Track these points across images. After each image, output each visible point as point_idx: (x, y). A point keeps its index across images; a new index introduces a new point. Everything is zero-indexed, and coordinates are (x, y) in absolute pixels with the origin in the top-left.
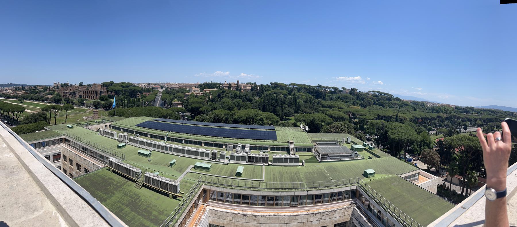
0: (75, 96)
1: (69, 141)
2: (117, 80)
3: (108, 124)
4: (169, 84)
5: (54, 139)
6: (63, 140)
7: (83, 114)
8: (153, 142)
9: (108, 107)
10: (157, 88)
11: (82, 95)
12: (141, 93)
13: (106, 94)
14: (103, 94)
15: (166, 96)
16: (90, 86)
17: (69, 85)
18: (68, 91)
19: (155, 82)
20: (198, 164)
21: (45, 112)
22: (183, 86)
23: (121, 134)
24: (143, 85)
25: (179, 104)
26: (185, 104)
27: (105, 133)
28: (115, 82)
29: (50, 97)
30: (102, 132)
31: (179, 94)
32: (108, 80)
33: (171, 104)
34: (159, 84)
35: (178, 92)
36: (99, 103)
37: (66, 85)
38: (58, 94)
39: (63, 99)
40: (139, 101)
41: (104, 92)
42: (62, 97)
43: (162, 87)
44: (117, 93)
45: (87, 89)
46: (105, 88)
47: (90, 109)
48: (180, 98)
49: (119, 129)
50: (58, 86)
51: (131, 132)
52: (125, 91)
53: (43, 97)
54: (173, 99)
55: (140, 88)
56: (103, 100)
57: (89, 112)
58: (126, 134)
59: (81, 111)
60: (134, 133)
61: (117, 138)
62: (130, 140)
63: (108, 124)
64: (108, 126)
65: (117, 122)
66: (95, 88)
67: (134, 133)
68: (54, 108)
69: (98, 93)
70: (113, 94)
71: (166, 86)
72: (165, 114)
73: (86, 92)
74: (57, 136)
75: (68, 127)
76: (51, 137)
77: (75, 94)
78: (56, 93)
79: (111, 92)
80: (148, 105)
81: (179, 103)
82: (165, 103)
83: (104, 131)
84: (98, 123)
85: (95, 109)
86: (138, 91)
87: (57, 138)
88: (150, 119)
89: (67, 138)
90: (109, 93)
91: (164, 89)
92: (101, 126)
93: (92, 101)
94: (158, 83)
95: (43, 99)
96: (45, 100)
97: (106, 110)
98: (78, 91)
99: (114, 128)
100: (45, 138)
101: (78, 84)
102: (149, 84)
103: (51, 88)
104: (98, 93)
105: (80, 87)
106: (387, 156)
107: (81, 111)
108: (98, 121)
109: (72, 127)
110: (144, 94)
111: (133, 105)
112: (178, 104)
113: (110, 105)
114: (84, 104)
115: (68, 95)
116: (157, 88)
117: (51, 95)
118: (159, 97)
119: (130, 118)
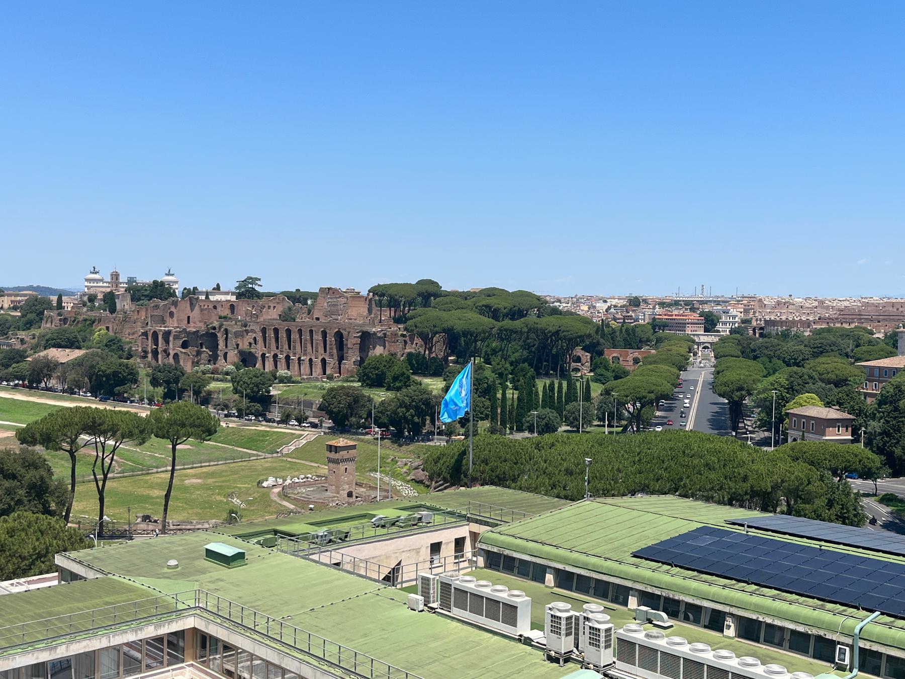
0: (213, 359)
1: (227, 647)
2: (461, 273)
3: (447, 537)
4: (751, 304)
5: (131, 637)
6: (186, 643)
7: (263, 460)
8: (487, 590)
9: (410, 422)
10: (681, 326)
11: (259, 349)
12: (595, 350)
13: (398, 348)
14: (379, 351)
15: (742, 370)
16: (298, 298)
17: (178, 289)
18: (172, 325)
19: (669, 294)
20: (212, 547)
21: (39, 448)
22: (846, 314)
23: (563, 609)
24: (601, 306)
25: (832, 423)
26: (875, 426)
27: (451, 596)
28: (447, 286)
29: (63, 356)
30: (435, 591)
31: (832, 364)
32: (406, 273)
33: (776, 421)
34: (690, 305)
35: (819, 351)
36: (356, 401)
37: (160, 290)
38: (114, 344)
39: (143, 373)
40: (587, 397)
41: (383, 340)
42: (135, 361)
43: (710, 323)
44: (460, 345)
45: (287, 316)
46: (387, 314)
47: (308, 435)
48: (836, 390)
49: (536, 572)
50: (110, 300)
51: (613, 593)
52: (506, 336)
53: (20, 356)
54: (792, 390)
55: (586, 321)
56: (377, 382)
57: (300, 453)
58: (596, 611)
59: (253, 442)
60: (633, 602)
61: (536, 635)
62: (626, 650)
63: (447, 537)
64: (448, 550)
65: (516, 527)
66: (332, 312)
67: (633, 602)
68: (94, 425)
69: (352, 341)
70: (439, 350)
71: (737, 313)
72: (767, 485)
73: (283, 334)
74: (147, 619)
75: (211, 554)
76: (116, 622)
77: (214, 347)
78: (99, 333)
79: (427, 339)
80: (637, 418)
81: (833, 413)
82: (736, 411)
83: (446, 587)
84: (391, 527)
85: (334, 431)
86: (574, 341)
87: (150, 632)
88: (717, 515)
89: (214, 630)
90: (416, 347)
91: (724, 329)
92: (409, 551)
93: (314, 387)
94: (686, 294)
95: (23, 367)
96: (34, 380)
97: (397, 438)
98: (234, 328)
99: (497, 561)
100: (75, 632)
101: (230, 284)
102: (635, 302)
103: (68, 305)
104: (352, 341)
105: (244, 308)
106: (540, 509)
107: (253, 442)
108: (390, 513)
109: (240, 556)
110: (610, 354)
111: (552, 414)
112: (824, 424)
113: (421, 413)
114: (266, 401)
115: (174, 347)
116: (681, 326)
117: (72, 344)
118: (701, 370)
119: (587, 505)
